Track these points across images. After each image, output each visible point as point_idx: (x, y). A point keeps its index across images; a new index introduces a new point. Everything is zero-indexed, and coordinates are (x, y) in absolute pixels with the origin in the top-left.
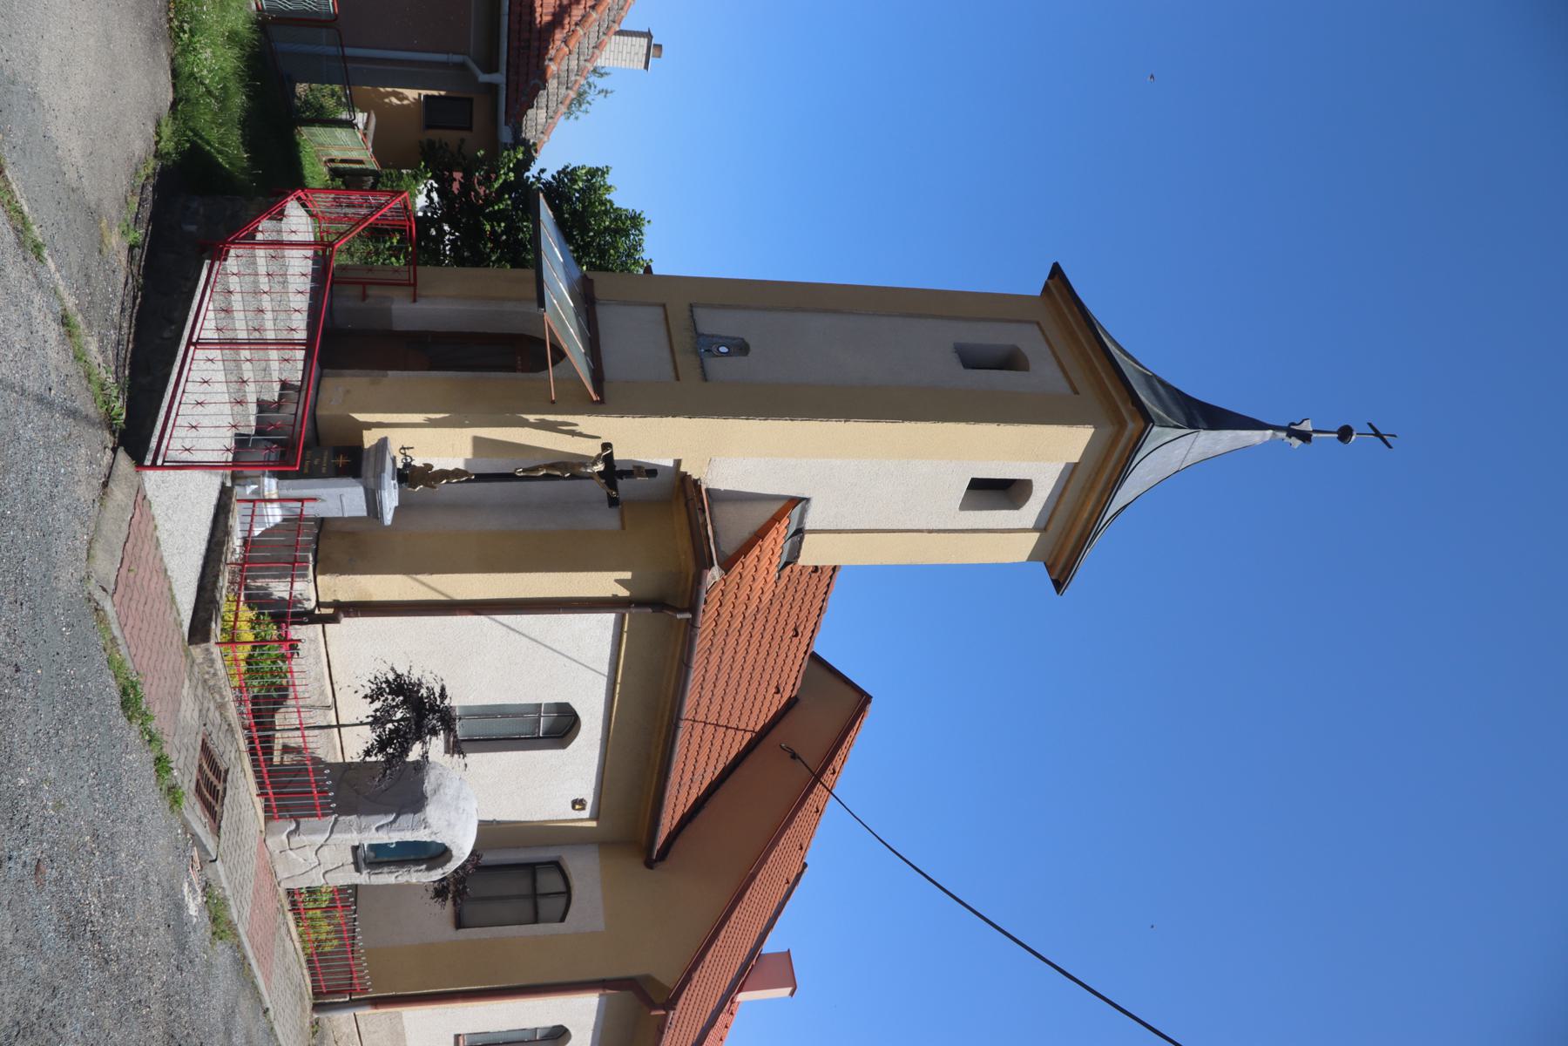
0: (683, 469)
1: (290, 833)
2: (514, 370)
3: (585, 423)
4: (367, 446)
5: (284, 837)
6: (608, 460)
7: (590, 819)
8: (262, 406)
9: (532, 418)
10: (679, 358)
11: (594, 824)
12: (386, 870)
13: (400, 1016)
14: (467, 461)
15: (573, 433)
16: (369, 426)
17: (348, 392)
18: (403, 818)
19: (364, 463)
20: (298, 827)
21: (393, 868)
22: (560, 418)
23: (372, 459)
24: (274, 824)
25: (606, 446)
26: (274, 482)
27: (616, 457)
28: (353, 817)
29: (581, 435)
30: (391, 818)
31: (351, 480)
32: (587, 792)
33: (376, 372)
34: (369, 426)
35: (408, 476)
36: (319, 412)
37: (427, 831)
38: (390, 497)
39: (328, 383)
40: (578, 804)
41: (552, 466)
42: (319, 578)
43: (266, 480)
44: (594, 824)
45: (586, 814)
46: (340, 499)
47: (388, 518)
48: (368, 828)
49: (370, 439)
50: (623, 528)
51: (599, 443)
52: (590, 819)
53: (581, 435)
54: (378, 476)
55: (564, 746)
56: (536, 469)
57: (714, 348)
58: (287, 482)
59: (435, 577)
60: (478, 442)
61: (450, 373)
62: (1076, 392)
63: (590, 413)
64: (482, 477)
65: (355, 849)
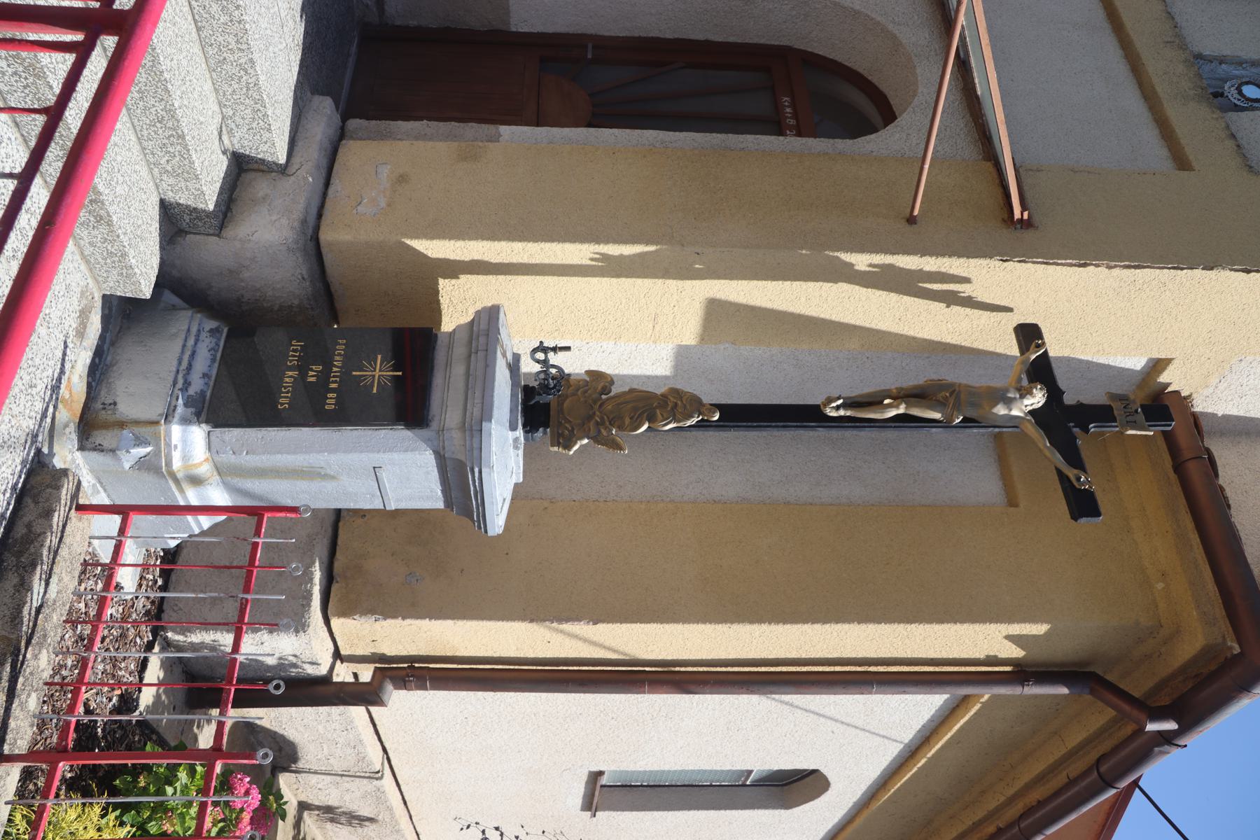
0: (1163, 378)
2: (778, 129)
3: (987, 276)
4: (448, 324)
6: (1041, 371)
8: (175, 222)
9: (861, 261)
10: (1174, 112)
13: (525, 374)
14: (682, 354)
15: (951, 299)
16: (454, 269)
17: (402, 179)
19: (438, 380)
22: (930, 264)
23: (458, 370)
25: (1028, 334)
26: (198, 433)
27: (1051, 354)
29: (969, 302)
31: (402, 434)
33: (472, 129)
34: (454, 269)
35: (552, 406)
36: (326, 236)
38: (504, 460)
39: (355, 154)
41: (917, 395)
42: (335, 622)
43: (176, 430)
46: (389, 471)
47: (497, 521)
49: (457, 305)
50: (1012, 502)
51: (1009, 322)
53: (969, 302)
54: (474, 428)
55: (788, 805)
56: (873, 401)
57: (1230, 90)
58: (234, 435)
59: (602, 627)
60: (718, 315)
61: (650, 135)
62: (1182, 162)
63: (1006, 255)
64: (738, 416)
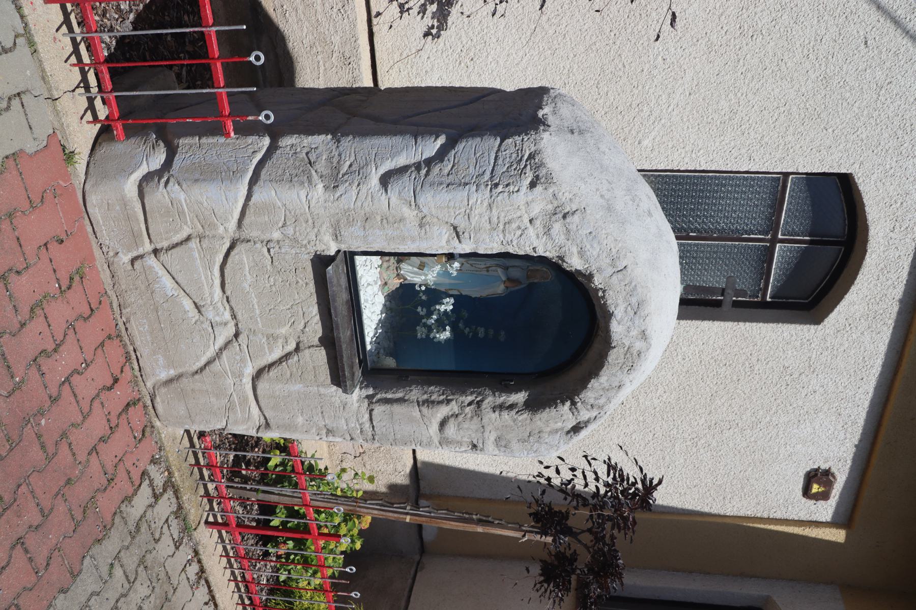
1: (148, 177)
5: (130, 186)
7: (834, 524)
11: (838, 536)
12: (415, 393)
18: (466, 148)
20: (168, 164)
21: (435, 393)
24: (122, 147)
28: (321, 141)
30: (431, 146)
32: (839, 453)
37: (537, 202)
40: (816, 481)
44: (838, 536)
45: (825, 510)
48: (358, 172)
52: (834, 524)
55: (817, 320)
65: (332, 277)
